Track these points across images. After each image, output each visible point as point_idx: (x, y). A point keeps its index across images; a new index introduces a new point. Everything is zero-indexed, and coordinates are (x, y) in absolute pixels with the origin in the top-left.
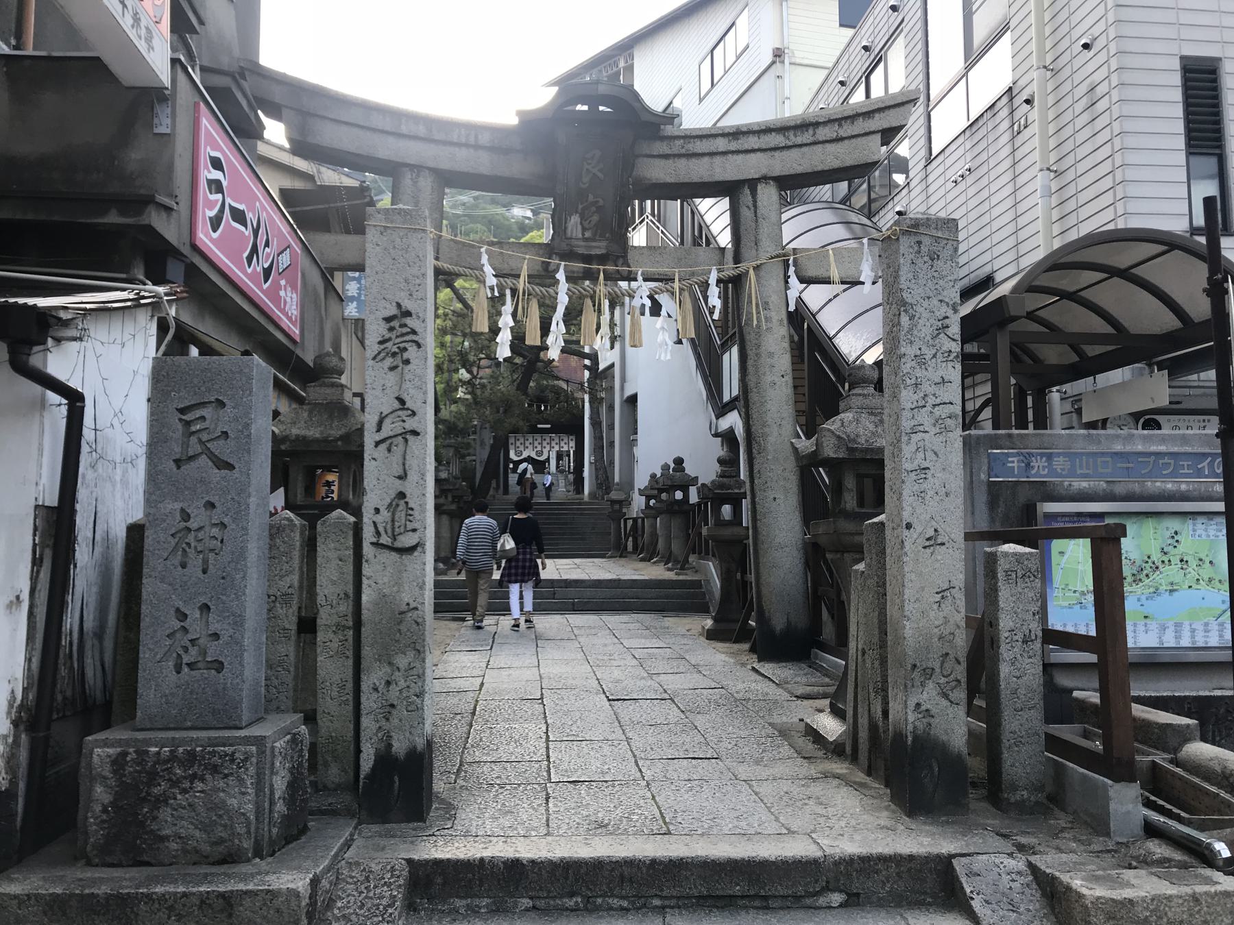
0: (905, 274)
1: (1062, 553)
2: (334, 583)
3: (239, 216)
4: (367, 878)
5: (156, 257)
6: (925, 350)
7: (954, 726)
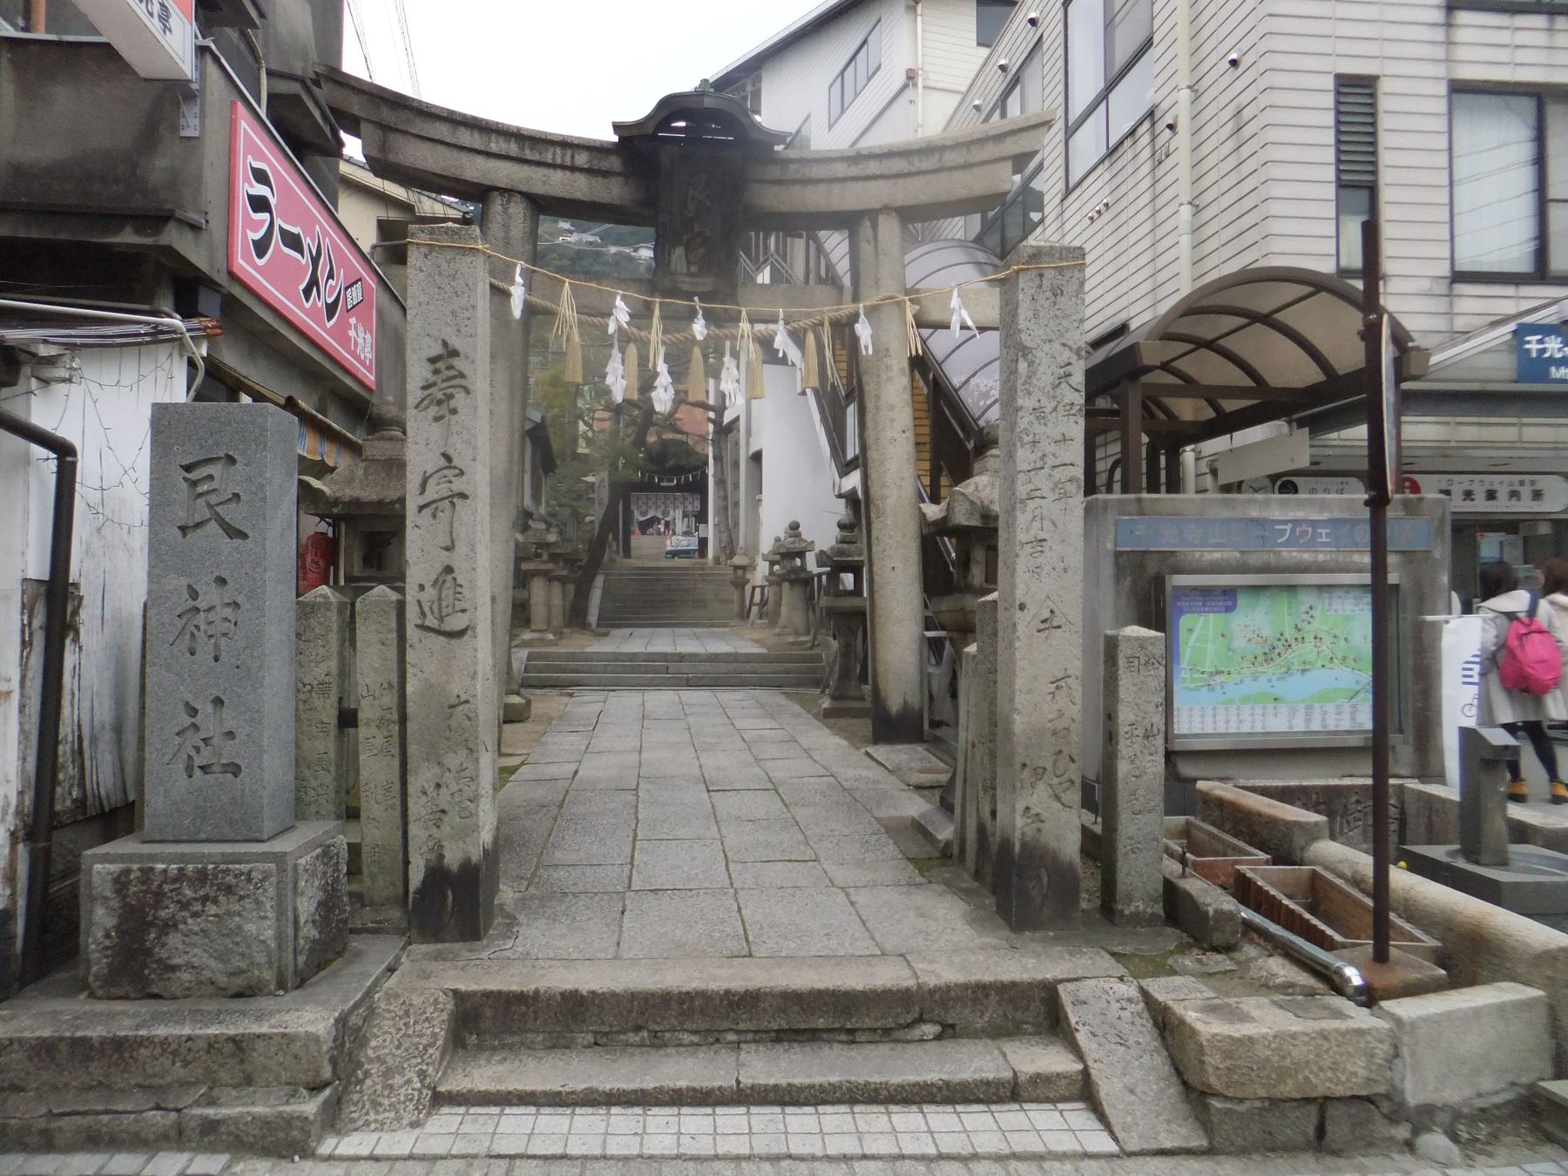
0: (1024, 312)
1: (1191, 630)
2: (376, 670)
3: (293, 242)
4: (407, 1013)
5: (188, 289)
6: (1045, 402)
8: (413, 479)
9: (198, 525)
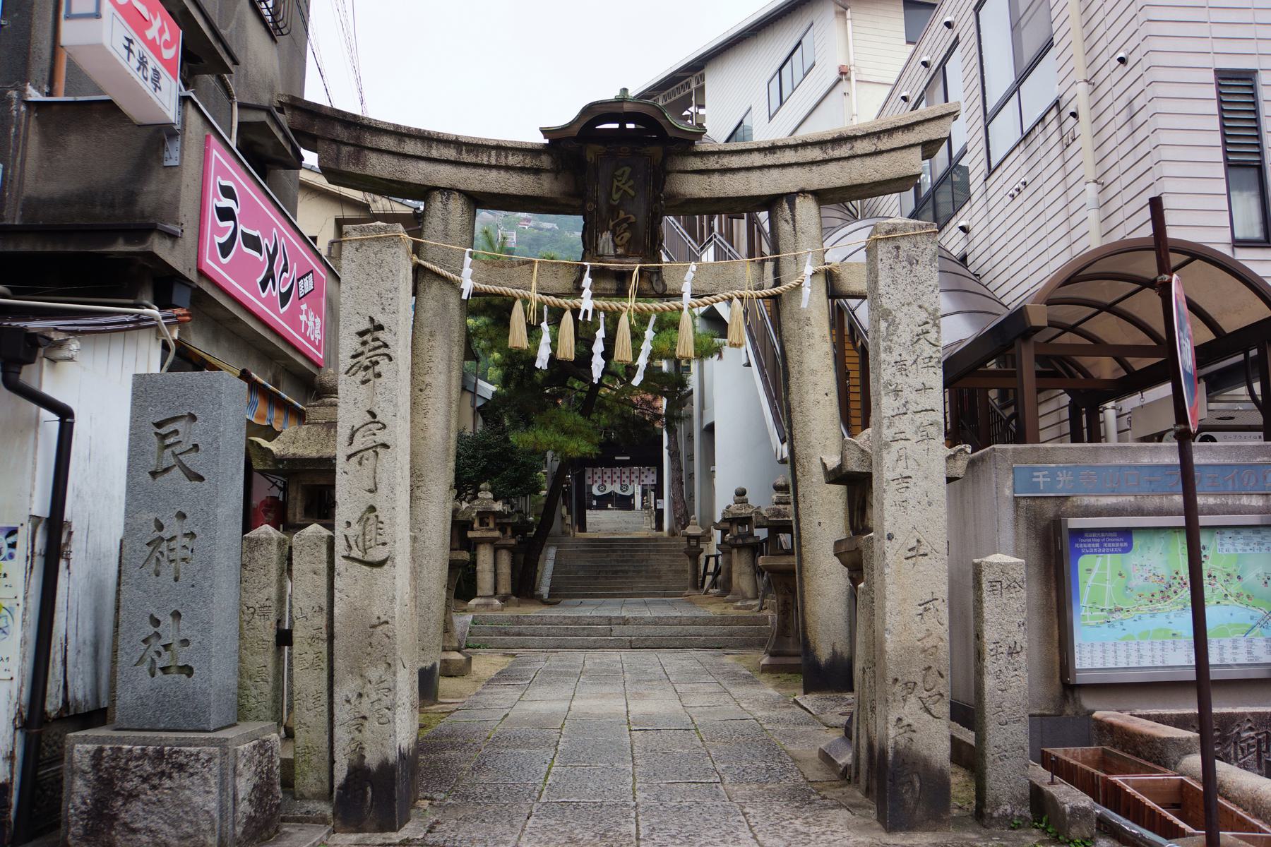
3: (253, 242)
7: (934, 738)
8: (343, 432)
9: (166, 470)
